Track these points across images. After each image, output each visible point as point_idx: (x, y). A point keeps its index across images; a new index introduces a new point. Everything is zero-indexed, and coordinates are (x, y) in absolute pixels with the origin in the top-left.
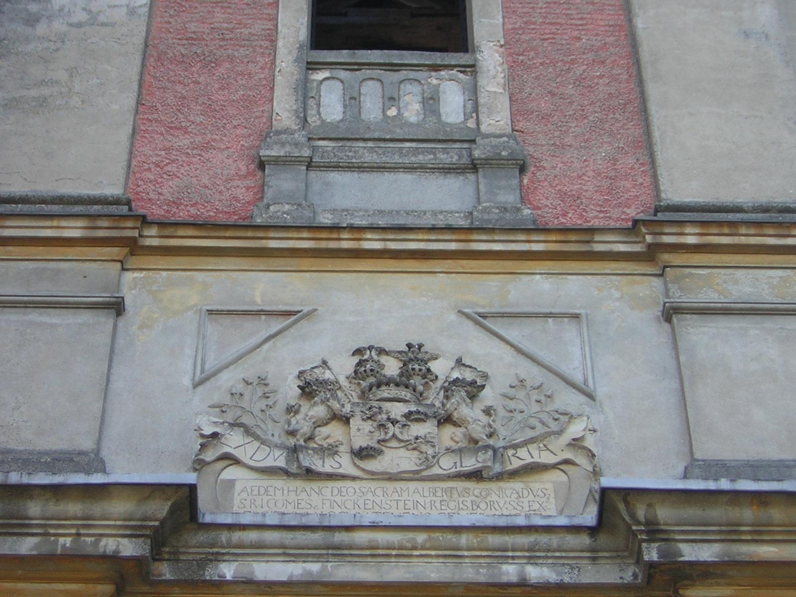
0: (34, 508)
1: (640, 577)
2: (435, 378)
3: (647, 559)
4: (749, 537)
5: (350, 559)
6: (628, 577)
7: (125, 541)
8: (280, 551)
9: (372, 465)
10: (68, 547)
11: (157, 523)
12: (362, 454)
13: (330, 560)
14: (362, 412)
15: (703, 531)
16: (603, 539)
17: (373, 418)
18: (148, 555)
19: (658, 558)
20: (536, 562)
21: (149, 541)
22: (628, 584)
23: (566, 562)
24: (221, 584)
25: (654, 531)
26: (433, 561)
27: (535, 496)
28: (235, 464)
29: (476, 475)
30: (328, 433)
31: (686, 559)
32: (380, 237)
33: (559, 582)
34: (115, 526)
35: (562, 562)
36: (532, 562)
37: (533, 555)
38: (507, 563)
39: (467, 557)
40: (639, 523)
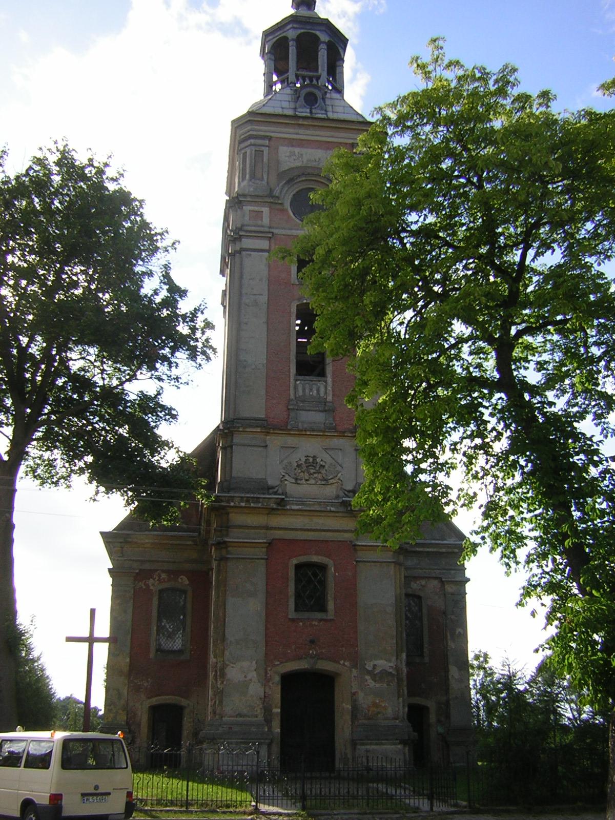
0: (261, 500)
9: (308, 482)
12: (307, 480)
28: (351, 517)
29: (324, 485)
37: (332, 506)
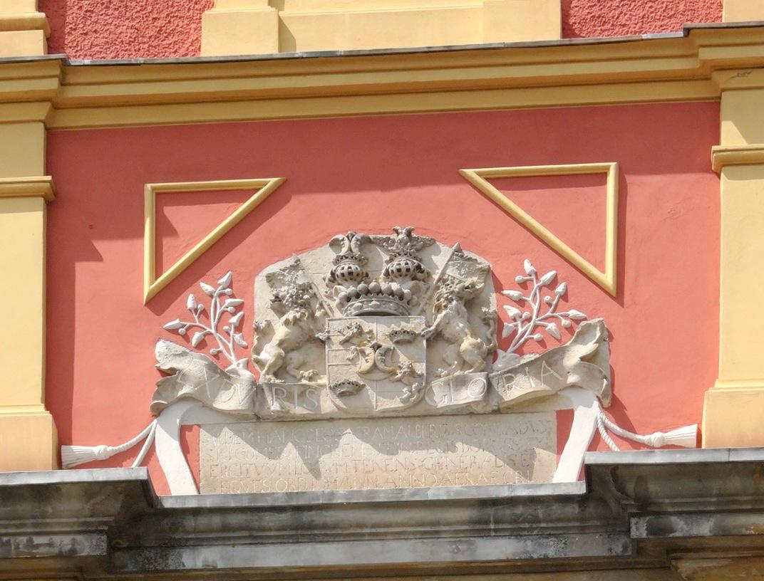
1: (630, 549)
2: (426, 275)
3: (635, 537)
4: (749, 507)
5: (321, 538)
6: (618, 549)
7: (79, 538)
8: (246, 533)
10: (52, 178)
11: (111, 519)
13: (300, 540)
14: (348, 299)
15: (699, 502)
16: (591, 509)
17: (351, 341)
18: (105, 554)
19: (647, 535)
20: (521, 534)
21: (104, 537)
22: (617, 556)
23: (552, 532)
24: (185, 574)
25: (645, 506)
26: (410, 537)
27: (534, 431)
30: (301, 359)
31: (677, 534)
32: (250, 542)
33: (542, 557)
34: (66, 524)
35: (548, 533)
36: (515, 533)
38: (488, 536)
39: (445, 531)
40: (628, 497)
